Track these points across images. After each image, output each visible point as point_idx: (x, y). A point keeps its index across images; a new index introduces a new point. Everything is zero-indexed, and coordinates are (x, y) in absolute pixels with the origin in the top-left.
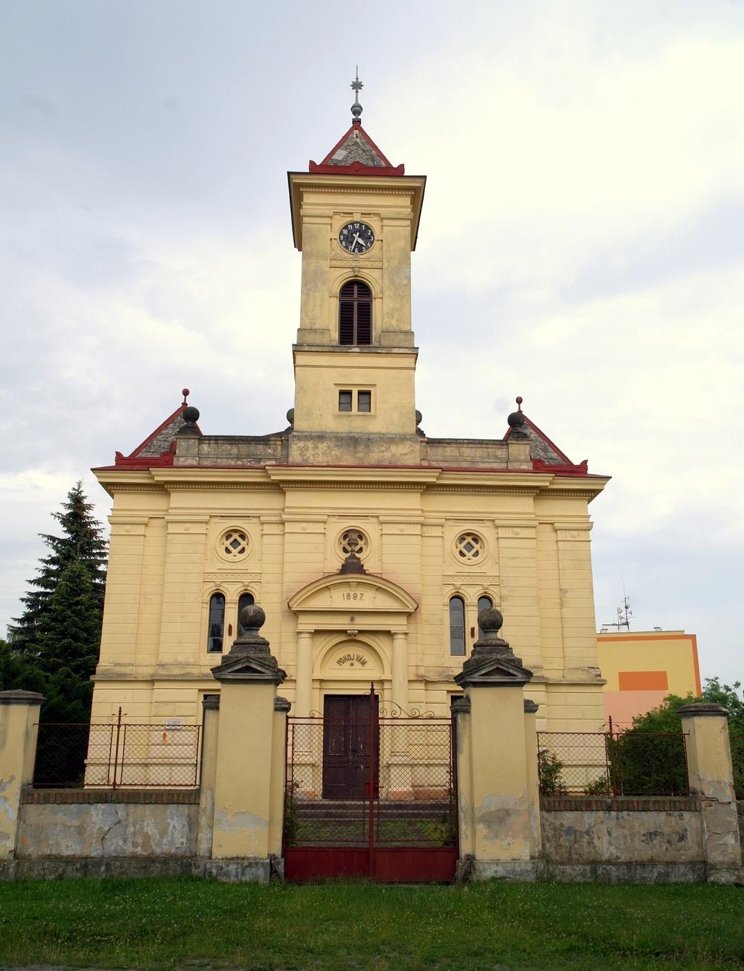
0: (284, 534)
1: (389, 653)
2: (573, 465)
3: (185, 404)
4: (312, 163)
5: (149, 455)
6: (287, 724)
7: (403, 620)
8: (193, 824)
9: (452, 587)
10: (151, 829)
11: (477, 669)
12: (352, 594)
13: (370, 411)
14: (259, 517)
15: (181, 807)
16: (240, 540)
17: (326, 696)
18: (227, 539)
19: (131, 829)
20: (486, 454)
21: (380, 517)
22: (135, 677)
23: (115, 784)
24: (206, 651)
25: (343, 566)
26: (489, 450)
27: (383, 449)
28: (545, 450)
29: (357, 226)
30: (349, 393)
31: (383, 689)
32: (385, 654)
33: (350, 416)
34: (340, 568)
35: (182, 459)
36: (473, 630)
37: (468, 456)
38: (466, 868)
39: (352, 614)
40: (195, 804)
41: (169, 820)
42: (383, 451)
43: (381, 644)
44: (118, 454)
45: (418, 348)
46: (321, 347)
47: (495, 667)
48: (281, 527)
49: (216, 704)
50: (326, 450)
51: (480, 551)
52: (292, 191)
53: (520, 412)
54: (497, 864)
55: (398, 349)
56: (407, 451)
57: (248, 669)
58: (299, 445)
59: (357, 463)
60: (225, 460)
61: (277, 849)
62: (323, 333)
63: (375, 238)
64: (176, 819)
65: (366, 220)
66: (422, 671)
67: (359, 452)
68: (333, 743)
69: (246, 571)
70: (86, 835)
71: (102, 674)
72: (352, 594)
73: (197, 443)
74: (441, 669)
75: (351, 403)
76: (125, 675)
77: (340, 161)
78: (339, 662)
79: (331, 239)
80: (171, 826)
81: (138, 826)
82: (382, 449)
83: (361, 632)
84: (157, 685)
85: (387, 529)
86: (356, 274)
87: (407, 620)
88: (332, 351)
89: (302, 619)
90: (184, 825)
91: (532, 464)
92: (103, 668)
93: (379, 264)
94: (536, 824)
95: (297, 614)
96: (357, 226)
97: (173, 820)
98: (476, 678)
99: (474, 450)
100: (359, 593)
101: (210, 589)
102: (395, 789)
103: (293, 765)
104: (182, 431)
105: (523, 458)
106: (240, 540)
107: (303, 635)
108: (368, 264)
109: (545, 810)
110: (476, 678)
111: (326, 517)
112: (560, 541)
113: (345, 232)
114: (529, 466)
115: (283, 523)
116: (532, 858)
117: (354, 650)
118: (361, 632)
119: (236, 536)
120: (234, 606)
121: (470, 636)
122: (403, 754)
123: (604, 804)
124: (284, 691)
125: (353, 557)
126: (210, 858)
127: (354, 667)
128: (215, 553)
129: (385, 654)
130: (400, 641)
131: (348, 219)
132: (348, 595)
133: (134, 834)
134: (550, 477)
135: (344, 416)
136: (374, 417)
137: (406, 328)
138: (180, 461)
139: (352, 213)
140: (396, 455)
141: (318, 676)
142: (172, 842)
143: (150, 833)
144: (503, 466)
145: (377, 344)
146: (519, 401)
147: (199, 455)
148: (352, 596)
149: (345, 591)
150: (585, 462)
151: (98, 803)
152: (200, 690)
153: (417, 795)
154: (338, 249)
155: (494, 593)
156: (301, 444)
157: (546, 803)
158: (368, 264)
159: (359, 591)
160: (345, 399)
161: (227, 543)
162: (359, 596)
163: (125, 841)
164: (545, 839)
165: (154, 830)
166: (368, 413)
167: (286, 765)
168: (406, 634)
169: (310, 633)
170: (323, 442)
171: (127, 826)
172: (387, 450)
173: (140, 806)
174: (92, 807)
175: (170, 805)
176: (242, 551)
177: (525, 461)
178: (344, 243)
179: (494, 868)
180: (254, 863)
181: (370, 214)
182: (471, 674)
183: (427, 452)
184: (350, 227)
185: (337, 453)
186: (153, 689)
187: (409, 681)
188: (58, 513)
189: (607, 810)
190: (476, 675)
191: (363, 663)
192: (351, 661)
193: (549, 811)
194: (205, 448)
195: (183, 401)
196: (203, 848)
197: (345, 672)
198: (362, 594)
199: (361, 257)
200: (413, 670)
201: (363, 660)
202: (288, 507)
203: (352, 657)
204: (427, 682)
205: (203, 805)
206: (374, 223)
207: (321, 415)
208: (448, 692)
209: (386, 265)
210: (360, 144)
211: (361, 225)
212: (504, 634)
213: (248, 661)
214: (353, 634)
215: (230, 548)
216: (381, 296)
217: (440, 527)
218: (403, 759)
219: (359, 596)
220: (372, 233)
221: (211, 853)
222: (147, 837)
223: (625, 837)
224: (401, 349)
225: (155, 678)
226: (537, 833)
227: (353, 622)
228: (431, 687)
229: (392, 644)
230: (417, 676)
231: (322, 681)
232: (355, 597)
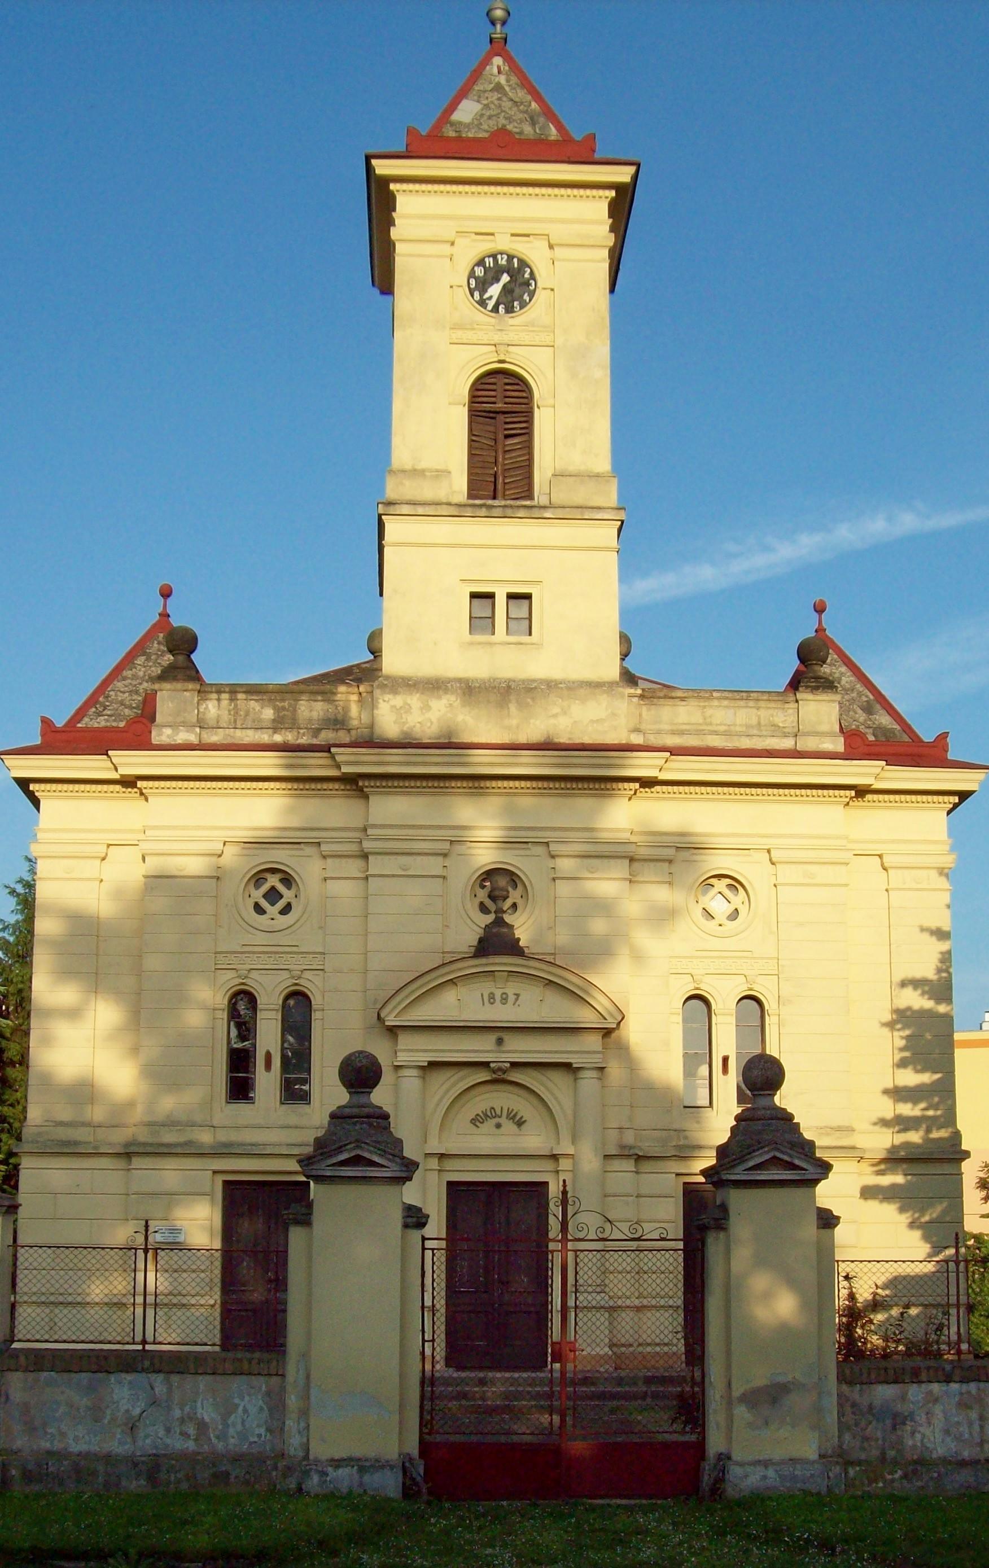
0: (367, 878)
1: (567, 1103)
2: (922, 741)
3: (165, 615)
4: (411, 132)
5: (101, 722)
6: (424, 1249)
8: (276, 1406)
10: (207, 1412)
11: (742, 1159)
12: (498, 994)
13: (530, 634)
14: (319, 844)
15: (255, 1381)
16: (281, 888)
19: (177, 1413)
21: (551, 845)
22: (95, 1148)
23: (144, 1342)
24: (224, 1100)
26: (762, 713)
27: (556, 710)
28: (868, 710)
29: (503, 261)
30: (490, 596)
32: (559, 1103)
34: (475, 943)
36: (725, 1060)
37: (720, 724)
38: (716, 1473)
39: (501, 1031)
40: (277, 1375)
41: (237, 1401)
42: (555, 716)
43: (550, 1085)
44: (46, 722)
46: (433, 507)
47: (771, 1155)
48: (360, 863)
51: (743, 911)
53: (820, 630)
54: (766, 1467)
57: (357, 1161)
58: (393, 702)
59: (505, 738)
60: (250, 732)
61: (413, 1447)
62: (437, 476)
63: (539, 284)
64: (247, 1398)
65: (522, 248)
66: (629, 1138)
68: (523, 1281)
69: (295, 949)
70: (106, 1421)
71: (32, 1142)
72: (498, 994)
73: (196, 699)
74: (664, 1134)
75: (493, 617)
76: (76, 1143)
77: (468, 126)
78: (474, 1121)
79: (451, 287)
80: (241, 1409)
81: (187, 1409)
83: (514, 1065)
84: (137, 1162)
86: (502, 357)
88: (458, 511)
89: (405, 1041)
90: (261, 1409)
91: (842, 739)
92: (35, 1130)
93: (548, 339)
94: (831, 1403)
96: (503, 261)
97: (243, 1399)
98: (738, 1174)
99: (732, 711)
101: (229, 981)
103: (156, 1305)
104: (167, 675)
105: (824, 728)
106: (281, 888)
108: (526, 338)
109: (846, 1383)
110: (738, 1174)
111: (447, 845)
112: (893, 889)
113: (479, 272)
114: (838, 745)
115: (365, 856)
116: (821, 1456)
117: (502, 1099)
119: (273, 881)
120: (272, 1015)
122: (590, 1289)
123: (940, 1373)
124: (411, 1194)
125: (499, 922)
126: (306, 1457)
127: (502, 1130)
128: (237, 916)
129: (559, 1103)
130: (588, 1081)
131: (485, 246)
132: (492, 997)
133: (182, 1421)
134: (876, 766)
135: (480, 643)
136: (538, 645)
138: (161, 735)
139: (492, 234)
142: (243, 1436)
143: (207, 1419)
144: (788, 744)
145: (544, 501)
146: (820, 609)
147: (202, 724)
148: (498, 997)
149: (486, 987)
150: (944, 736)
151: (121, 1371)
152: (215, 1172)
153: (618, 1361)
154: (465, 305)
155: (313, 986)
156: (398, 701)
157: (848, 1372)
159: (511, 989)
160: (482, 608)
162: (511, 998)
163: (168, 1430)
164: (843, 1427)
165: (212, 1415)
166: (526, 639)
167: (423, 1307)
169: (422, 1068)
170: (439, 698)
171: (169, 1409)
172: (565, 713)
173: (189, 1378)
174: (113, 1378)
175: (238, 1377)
176: (286, 910)
177: (830, 734)
178: (477, 295)
179: (760, 1471)
180: (378, 1465)
181: (528, 236)
182: (733, 1166)
183: (640, 715)
184: (489, 262)
186: (129, 1170)
187: (605, 1156)
188: (106, 940)
189: (945, 1381)
190: (740, 1169)
191: (520, 1123)
193: (850, 1383)
194: (212, 708)
195: (160, 610)
196: (294, 1443)
197: (484, 1141)
198: (517, 995)
200: (613, 1135)
201: (518, 1118)
202: (374, 826)
203: (498, 1112)
204: (639, 1158)
205: (291, 1376)
206: (535, 254)
210: (507, 89)
211: (510, 258)
212: (784, 1098)
213: (357, 1147)
214: (500, 1069)
215: (264, 904)
216: (551, 402)
217: (667, 864)
218: (598, 1298)
219: (511, 998)
220: (532, 273)
221: (307, 1451)
222: (202, 1426)
223: (970, 1424)
225: (132, 1149)
226: (832, 1418)
228: (647, 1166)
229: (575, 1089)
230: (623, 1147)
231: (442, 1156)
232: (504, 999)
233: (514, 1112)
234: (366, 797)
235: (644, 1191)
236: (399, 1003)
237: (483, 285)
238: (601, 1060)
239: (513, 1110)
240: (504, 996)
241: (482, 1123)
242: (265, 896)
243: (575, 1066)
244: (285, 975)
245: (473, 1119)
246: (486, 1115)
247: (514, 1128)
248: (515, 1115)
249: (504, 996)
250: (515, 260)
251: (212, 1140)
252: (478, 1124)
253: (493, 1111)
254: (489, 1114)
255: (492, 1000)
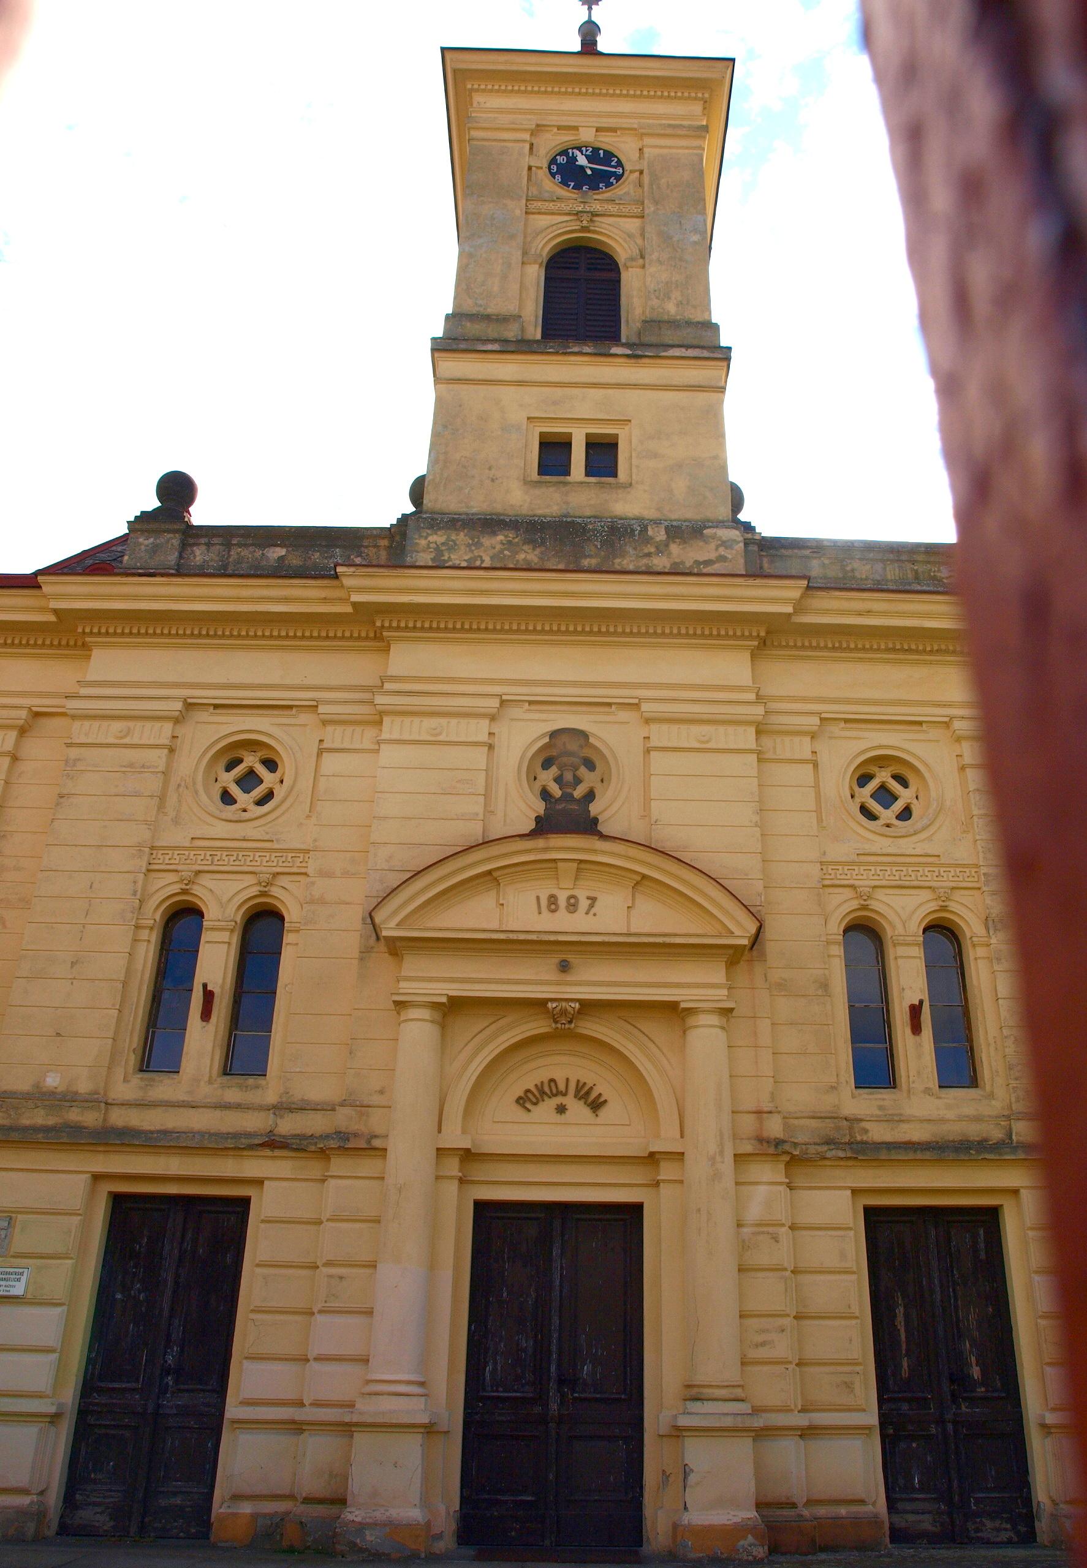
7: (715, 973)
9: (848, 893)
17: (481, 1207)
18: (229, 768)
20: (910, 575)
25: (538, 819)
31: (657, 1184)
33: (566, 484)
35: (1007, 1050)
42: (649, 555)
45: (730, 349)
49: (737, 1159)
50: (501, 551)
52: (452, 111)
55: (683, 350)
56: (713, 556)
65: (607, 142)
66: (774, 1128)
67: (586, 557)
78: (521, 1101)
82: (646, 551)
85: (661, 735)
87: (727, 973)
89: (414, 965)
93: (636, 210)
95: (396, 948)
100: (582, 895)
102: (699, 1516)
107: (414, 1013)
118: (588, 1007)
121: (908, 1030)
132: (553, 900)
137: (699, 317)
140: (682, 563)
141: (455, 1137)
148: (562, 902)
152: (97, 1178)
156: (438, 538)
158: (610, 207)
161: (228, 779)
162: (584, 904)
168: (727, 1012)
169: (435, 1006)
170: (494, 533)
185: (529, 557)
191: (596, 1105)
192: (559, 1100)
198: (593, 900)
199: (596, 197)
201: (593, 1095)
203: (562, 1087)
207: (493, 480)
208: (855, 1192)
209: (650, 208)
214: (564, 1012)
215: (235, 790)
219: (584, 904)
224: (690, 351)
227: (569, 978)
233: (586, 1089)
234: (387, 650)
235: (803, 1219)
236: (412, 898)
237: (578, 268)
238: (725, 998)
239: (585, 1083)
240: (572, 901)
241: (535, 1104)
242: (239, 782)
243: (683, 1005)
244: (250, 880)
245: (520, 1098)
246: (542, 1092)
247: (586, 1112)
248: (588, 1093)
249: (572, 901)
250: (601, 152)
251: (100, 1122)
252: (528, 1105)
253: (552, 1084)
254: (546, 1089)
255: (553, 907)
